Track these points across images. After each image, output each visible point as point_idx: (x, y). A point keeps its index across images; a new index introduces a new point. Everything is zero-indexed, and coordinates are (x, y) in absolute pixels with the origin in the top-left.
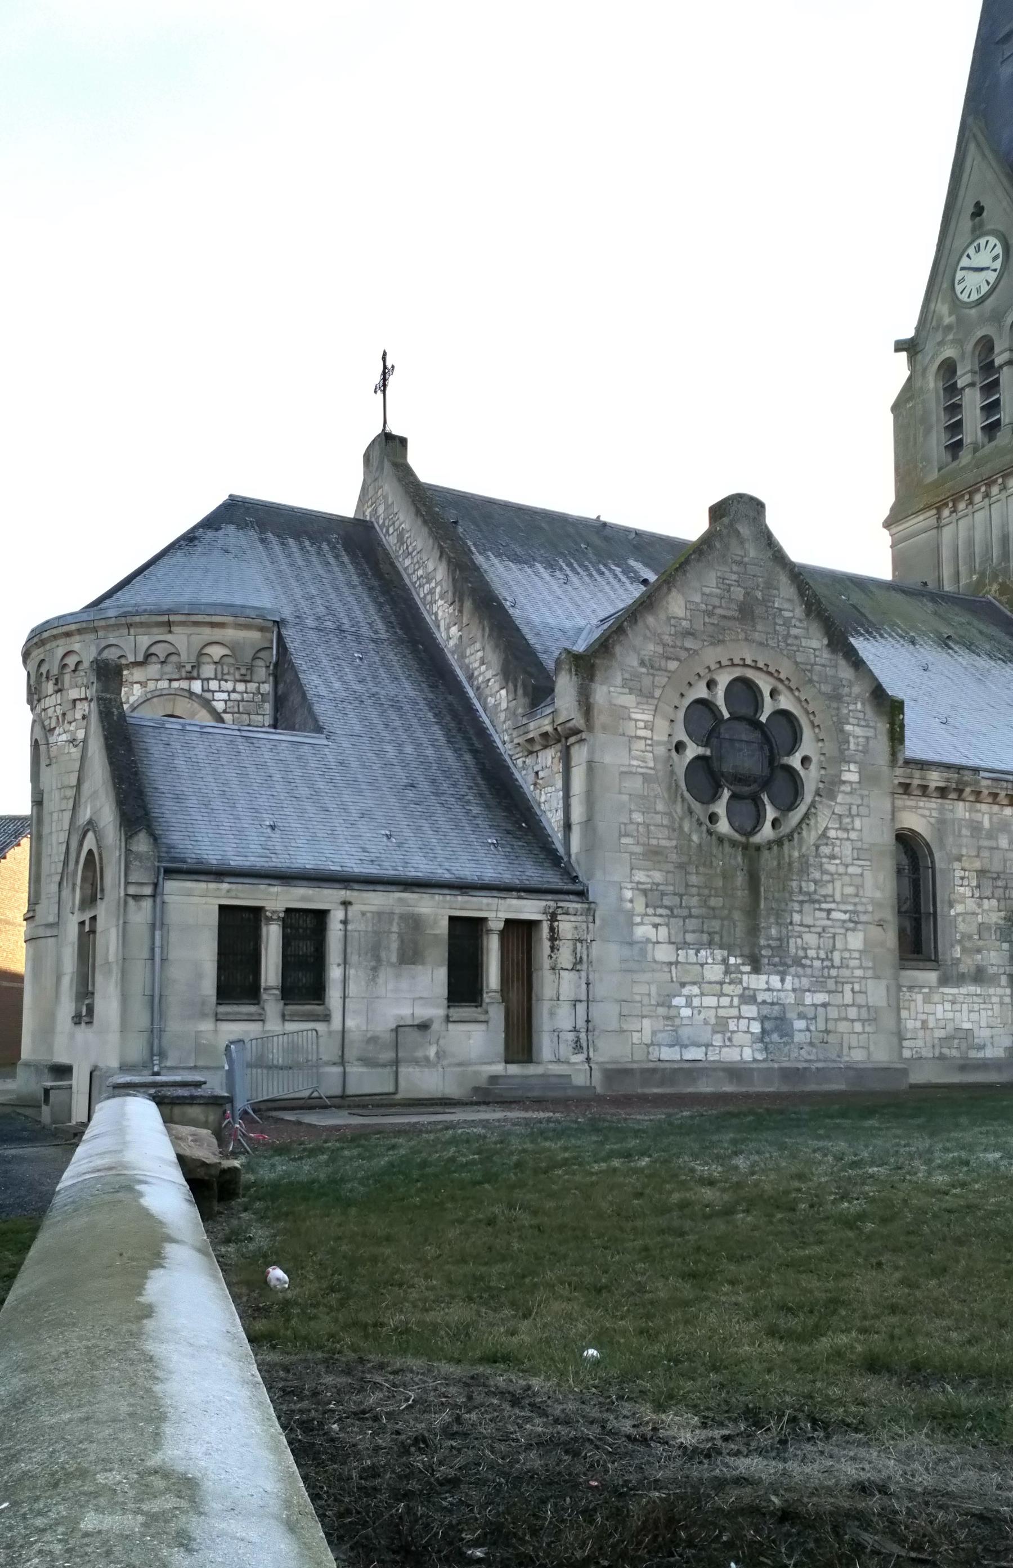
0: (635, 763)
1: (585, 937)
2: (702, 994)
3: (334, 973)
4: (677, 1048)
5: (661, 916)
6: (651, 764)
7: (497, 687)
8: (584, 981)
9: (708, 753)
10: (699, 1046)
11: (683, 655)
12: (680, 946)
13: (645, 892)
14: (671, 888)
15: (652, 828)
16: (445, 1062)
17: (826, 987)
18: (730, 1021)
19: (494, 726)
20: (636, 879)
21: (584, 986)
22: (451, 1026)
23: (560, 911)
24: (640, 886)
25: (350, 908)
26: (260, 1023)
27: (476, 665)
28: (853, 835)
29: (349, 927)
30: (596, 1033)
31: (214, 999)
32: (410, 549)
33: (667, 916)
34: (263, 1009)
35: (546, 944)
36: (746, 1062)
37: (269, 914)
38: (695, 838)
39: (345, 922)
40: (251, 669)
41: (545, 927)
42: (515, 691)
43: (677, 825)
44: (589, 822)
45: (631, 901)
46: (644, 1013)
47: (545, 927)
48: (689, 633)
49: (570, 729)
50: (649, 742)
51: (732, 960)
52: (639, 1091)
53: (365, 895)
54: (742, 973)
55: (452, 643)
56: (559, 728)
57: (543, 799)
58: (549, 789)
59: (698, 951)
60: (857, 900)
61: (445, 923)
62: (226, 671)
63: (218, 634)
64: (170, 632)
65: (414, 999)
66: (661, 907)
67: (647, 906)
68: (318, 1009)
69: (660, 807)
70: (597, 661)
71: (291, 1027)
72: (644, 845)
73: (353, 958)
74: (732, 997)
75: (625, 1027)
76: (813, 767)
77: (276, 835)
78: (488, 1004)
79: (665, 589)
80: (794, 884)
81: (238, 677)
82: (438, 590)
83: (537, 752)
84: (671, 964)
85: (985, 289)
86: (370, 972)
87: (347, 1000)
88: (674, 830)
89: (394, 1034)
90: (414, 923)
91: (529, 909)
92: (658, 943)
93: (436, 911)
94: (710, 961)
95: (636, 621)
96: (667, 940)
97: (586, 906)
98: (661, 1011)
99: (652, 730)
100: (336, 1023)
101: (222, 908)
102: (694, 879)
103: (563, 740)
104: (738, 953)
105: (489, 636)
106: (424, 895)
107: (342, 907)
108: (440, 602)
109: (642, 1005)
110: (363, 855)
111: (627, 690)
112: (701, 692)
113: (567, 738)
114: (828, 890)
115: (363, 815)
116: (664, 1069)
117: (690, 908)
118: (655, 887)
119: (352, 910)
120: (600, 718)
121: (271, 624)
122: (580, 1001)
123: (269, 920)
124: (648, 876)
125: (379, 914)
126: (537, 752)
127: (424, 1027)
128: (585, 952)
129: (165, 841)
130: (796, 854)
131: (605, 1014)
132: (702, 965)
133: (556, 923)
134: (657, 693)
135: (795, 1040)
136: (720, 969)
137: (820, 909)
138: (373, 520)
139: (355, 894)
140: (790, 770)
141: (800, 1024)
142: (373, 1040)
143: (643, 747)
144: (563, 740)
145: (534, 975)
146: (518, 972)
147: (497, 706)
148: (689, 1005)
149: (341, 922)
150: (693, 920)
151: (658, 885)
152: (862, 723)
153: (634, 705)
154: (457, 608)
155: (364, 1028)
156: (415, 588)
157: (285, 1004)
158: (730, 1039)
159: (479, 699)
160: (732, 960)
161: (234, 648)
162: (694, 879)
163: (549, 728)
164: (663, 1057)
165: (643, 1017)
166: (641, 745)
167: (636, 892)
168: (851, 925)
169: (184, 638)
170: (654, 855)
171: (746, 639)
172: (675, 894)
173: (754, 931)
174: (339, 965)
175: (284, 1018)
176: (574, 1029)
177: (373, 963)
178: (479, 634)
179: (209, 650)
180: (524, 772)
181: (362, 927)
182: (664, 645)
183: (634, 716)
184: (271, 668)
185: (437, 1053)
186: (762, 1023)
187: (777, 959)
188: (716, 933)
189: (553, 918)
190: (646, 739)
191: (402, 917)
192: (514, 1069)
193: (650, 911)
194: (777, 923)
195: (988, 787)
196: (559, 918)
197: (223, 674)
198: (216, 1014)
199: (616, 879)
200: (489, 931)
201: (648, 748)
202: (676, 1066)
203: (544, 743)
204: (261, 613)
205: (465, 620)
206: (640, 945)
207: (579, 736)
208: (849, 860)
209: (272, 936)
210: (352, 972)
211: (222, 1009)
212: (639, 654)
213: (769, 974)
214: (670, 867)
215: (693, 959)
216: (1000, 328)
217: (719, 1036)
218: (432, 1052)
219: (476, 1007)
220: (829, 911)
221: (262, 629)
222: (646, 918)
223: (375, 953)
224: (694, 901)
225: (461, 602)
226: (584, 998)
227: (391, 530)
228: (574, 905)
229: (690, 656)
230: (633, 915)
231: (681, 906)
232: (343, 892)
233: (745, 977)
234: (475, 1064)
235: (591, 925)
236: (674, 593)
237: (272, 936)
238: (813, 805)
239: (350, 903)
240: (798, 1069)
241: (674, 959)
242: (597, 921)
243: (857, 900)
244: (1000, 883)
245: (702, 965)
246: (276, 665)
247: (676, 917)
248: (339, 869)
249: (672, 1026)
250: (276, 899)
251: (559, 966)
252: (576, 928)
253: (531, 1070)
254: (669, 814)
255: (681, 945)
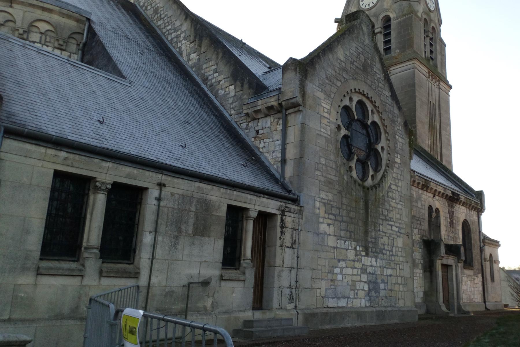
0: (322, 130)
1: (297, 228)
2: (347, 267)
3: (147, 239)
4: (335, 299)
5: (331, 219)
6: (329, 133)
7: (227, 84)
8: (296, 255)
9: (349, 134)
10: (345, 298)
11: (343, 80)
12: (338, 238)
13: (325, 204)
14: (335, 204)
15: (329, 168)
16: (217, 311)
17: (390, 266)
18: (357, 283)
19: (223, 106)
20: (321, 196)
21: (296, 258)
22: (223, 283)
23: (287, 209)
24: (323, 201)
25: (163, 189)
26: (79, 278)
27: (212, 72)
28: (399, 189)
29: (162, 204)
30: (300, 289)
31: (37, 254)
32: (163, 16)
33: (334, 220)
34: (83, 266)
35: (279, 229)
36: (363, 308)
37: (98, 184)
38: (345, 178)
39: (159, 199)
40: (66, 42)
41: (279, 218)
42: (242, 86)
43: (339, 169)
44: (300, 160)
45: (319, 209)
46: (323, 277)
47: (279, 218)
48: (345, 70)
49: (293, 103)
50: (328, 121)
51: (358, 248)
52: (320, 327)
53: (175, 180)
54: (362, 256)
55: (191, 63)
56: (283, 103)
57: (261, 146)
58: (268, 140)
59: (345, 242)
60: (400, 222)
61: (224, 209)
62: (48, 40)
63: (46, 16)
64: (11, 6)
65: (201, 262)
66: (331, 214)
67: (325, 213)
68: (130, 267)
69: (332, 158)
70: (309, 69)
71: (105, 282)
72: (325, 177)
73: (162, 228)
74: (358, 269)
75: (314, 286)
76: (385, 152)
77: (104, 128)
78: (245, 267)
79: (336, 43)
80: (380, 210)
81: (56, 45)
82: (183, 35)
83: (258, 119)
84: (334, 248)
85: (372, 5)
86: (173, 240)
87: (154, 261)
88: (337, 172)
89: (185, 289)
90: (206, 206)
91: (271, 206)
92: (329, 235)
93: (220, 199)
94: (350, 248)
95: (325, 55)
96: (333, 234)
97: (299, 208)
98: (330, 276)
99: (330, 114)
100: (143, 281)
101: (57, 174)
102: (345, 201)
103: (284, 111)
104: (360, 245)
105: (222, 57)
106: (214, 187)
107: (157, 187)
108: (184, 42)
109: (322, 272)
110: (170, 154)
111: (320, 90)
112: (346, 102)
113: (286, 110)
114: (391, 215)
115: (163, 131)
116: (331, 313)
117: (342, 216)
118: (329, 202)
119: (166, 191)
120: (309, 101)
121: (85, 19)
122: (294, 268)
123: (97, 189)
124: (327, 195)
125: (184, 196)
126: (258, 119)
127: (206, 283)
128: (297, 237)
129: (5, 108)
130: (381, 194)
131: (305, 275)
132: (347, 250)
133: (284, 217)
134: (332, 96)
135: (381, 295)
136: (353, 252)
137: (389, 225)
138: (136, 3)
139: (169, 179)
140: (377, 150)
141: (382, 286)
142: (170, 294)
143: (326, 123)
144: (284, 111)
145: (267, 250)
146: (258, 246)
147: (225, 95)
148: (341, 273)
149: (156, 198)
150: (344, 224)
151: (330, 201)
152: (401, 136)
153: (323, 99)
154: (197, 44)
155: (164, 284)
156: (165, 36)
157: (103, 262)
158: (357, 294)
159: (211, 92)
160: (358, 248)
161: (56, 28)
162: (345, 201)
163: (275, 104)
164: (330, 305)
165: (322, 279)
166: (325, 121)
167: (321, 203)
168: (398, 234)
169: (21, 13)
170: (329, 183)
171: (365, 82)
172: (337, 208)
173: (366, 233)
174: (150, 232)
175: (101, 274)
176: (290, 287)
177: (176, 233)
178: (214, 57)
179: (37, 24)
180: (246, 131)
181: (171, 205)
182: (336, 72)
183: (323, 104)
184: (81, 45)
185: (212, 304)
186: (369, 285)
187: (374, 249)
188: (352, 232)
189: (283, 214)
190: (327, 118)
191: (199, 201)
192: (258, 315)
193: (327, 216)
194: (375, 230)
195: (418, 180)
196: (286, 214)
197: (46, 41)
198: (38, 268)
199: (313, 195)
200: (248, 218)
201: (328, 124)
202: (336, 311)
203: (267, 112)
204: (79, 11)
205: (203, 50)
206: (322, 235)
207: (296, 109)
208: (397, 201)
209: (98, 205)
210: (160, 238)
211: (45, 264)
212: (326, 73)
213: (372, 257)
214: (335, 192)
215: (343, 247)
216: (377, 20)
217: (352, 292)
218: (208, 303)
219: (236, 269)
220: (392, 226)
221: (78, 21)
222: (325, 219)
223: (178, 224)
224: (345, 213)
225: (201, 41)
226: (295, 266)
227: (149, 8)
228: (293, 207)
229: (345, 81)
230: (319, 217)
231: (339, 215)
232: (160, 176)
233: (363, 258)
234: (235, 312)
235: (300, 220)
236: (340, 47)
237: (98, 205)
238: (386, 171)
239: (164, 185)
240: (382, 311)
241: (335, 246)
242: (304, 218)
243: (400, 222)
244: (419, 222)
245: (347, 250)
246: (85, 45)
247: (337, 221)
248: (156, 159)
249: (334, 285)
250: (107, 173)
251: (285, 244)
252: (294, 221)
253: (269, 315)
254: (336, 162)
255: (339, 238)
